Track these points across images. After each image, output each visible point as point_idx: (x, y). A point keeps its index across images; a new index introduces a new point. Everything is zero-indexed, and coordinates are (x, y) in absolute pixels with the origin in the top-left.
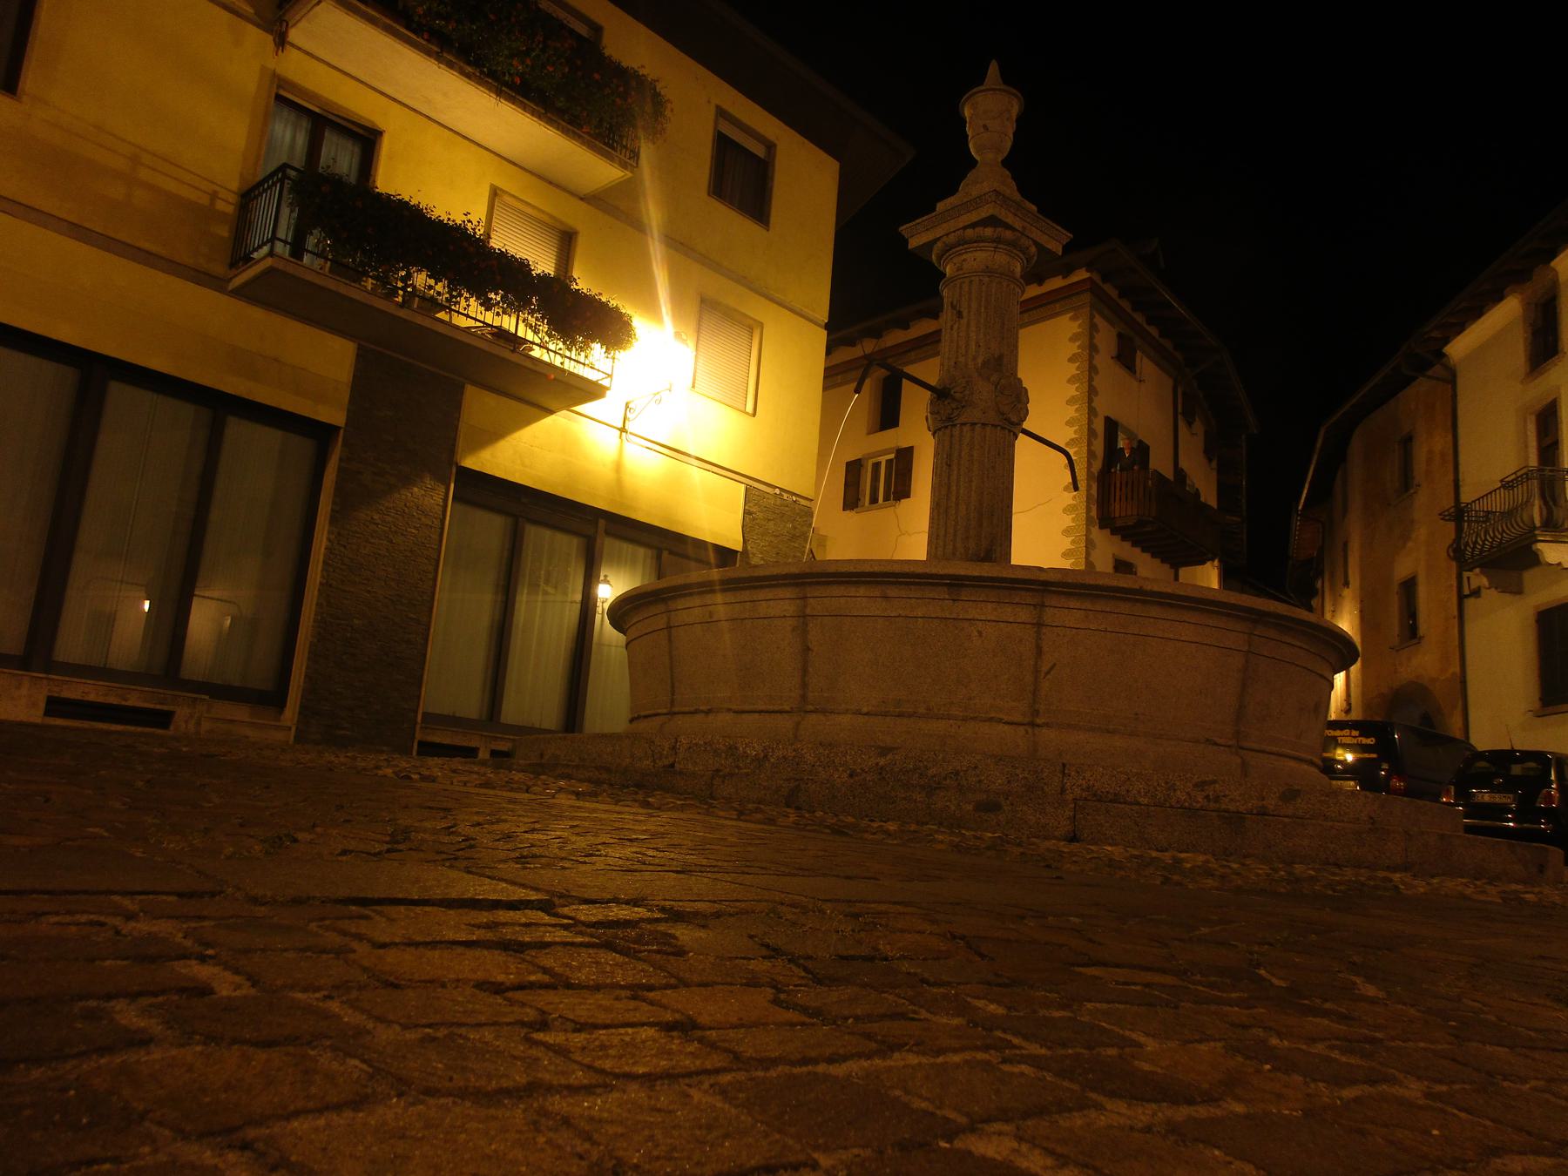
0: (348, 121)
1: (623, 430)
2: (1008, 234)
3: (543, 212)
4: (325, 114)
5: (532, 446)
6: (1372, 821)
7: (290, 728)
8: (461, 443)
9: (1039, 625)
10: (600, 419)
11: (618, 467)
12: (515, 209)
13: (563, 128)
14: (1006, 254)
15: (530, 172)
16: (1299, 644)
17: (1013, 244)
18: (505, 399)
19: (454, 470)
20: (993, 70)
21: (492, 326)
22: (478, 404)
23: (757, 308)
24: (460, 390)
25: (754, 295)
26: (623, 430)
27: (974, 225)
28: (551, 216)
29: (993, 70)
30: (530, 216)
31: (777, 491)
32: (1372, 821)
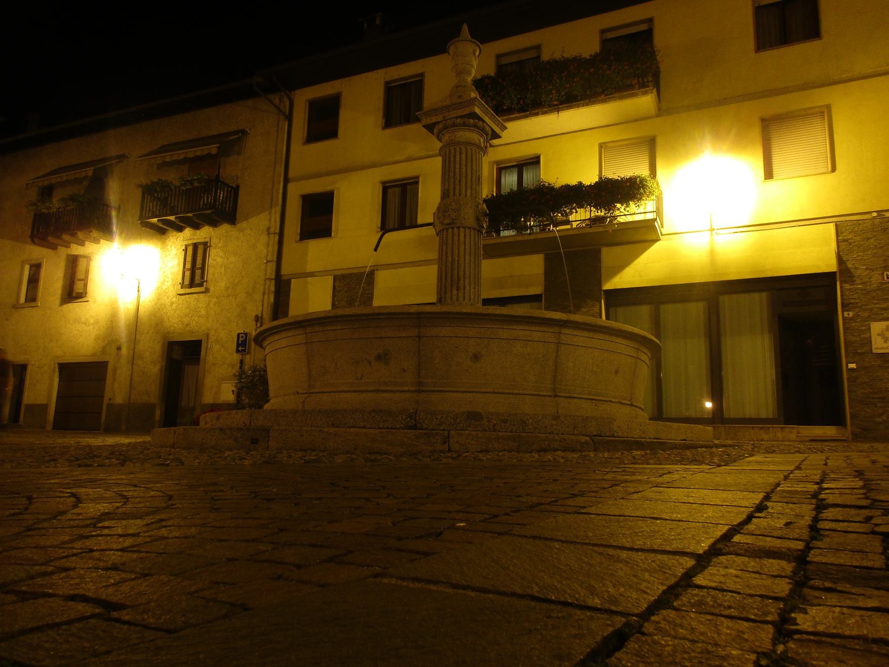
0: (526, 160)
1: (712, 230)
2: (441, 125)
3: (631, 139)
4: (518, 163)
5: (654, 263)
6: (244, 425)
7: (185, 429)
8: (603, 280)
9: (419, 337)
10: (687, 231)
11: (712, 253)
12: (621, 146)
13: (619, 97)
14: (448, 133)
15: (622, 123)
16: (339, 327)
17: (445, 128)
18: (626, 246)
19: (602, 293)
20: (465, 29)
21: (585, 220)
22: (608, 255)
23: (819, 97)
24: (598, 252)
25: (815, 90)
26: (712, 230)
27: (461, 117)
28: (637, 138)
29: (465, 29)
30: (627, 145)
31: (875, 214)
32: (244, 425)
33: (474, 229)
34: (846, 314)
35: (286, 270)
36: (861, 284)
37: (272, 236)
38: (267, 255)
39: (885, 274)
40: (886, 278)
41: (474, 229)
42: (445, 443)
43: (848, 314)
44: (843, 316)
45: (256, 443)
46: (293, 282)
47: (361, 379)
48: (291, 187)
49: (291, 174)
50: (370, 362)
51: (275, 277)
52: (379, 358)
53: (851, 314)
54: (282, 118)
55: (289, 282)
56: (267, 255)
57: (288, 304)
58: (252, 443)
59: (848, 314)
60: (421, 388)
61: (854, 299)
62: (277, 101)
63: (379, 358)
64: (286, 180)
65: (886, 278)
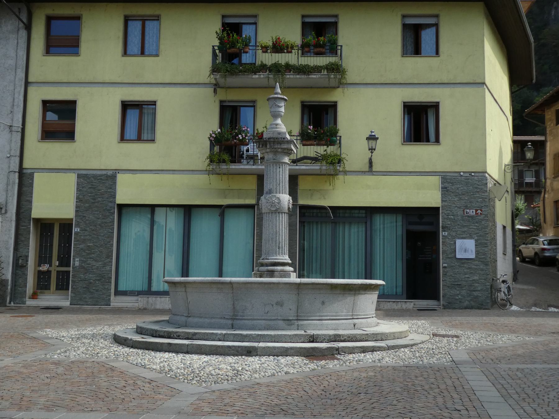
33: (286, 213)
34: (444, 233)
35: (26, 165)
36: (453, 215)
37: (14, 134)
38: (11, 150)
39: (465, 210)
40: (465, 213)
41: (286, 213)
42: (337, 350)
43: (445, 234)
44: (442, 235)
45: (251, 353)
46: (36, 175)
47: (267, 313)
48: (32, 90)
49: (31, 79)
50: (273, 305)
51: (19, 170)
52: (277, 303)
53: (446, 233)
54: (21, 25)
55: (32, 176)
56: (11, 150)
57: (32, 193)
58: (248, 353)
59: (445, 234)
60: (299, 318)
61: (448, 224)
62: (16, 10)
63: (277, 303)
64: (27, 83)
65: (465, 213)
